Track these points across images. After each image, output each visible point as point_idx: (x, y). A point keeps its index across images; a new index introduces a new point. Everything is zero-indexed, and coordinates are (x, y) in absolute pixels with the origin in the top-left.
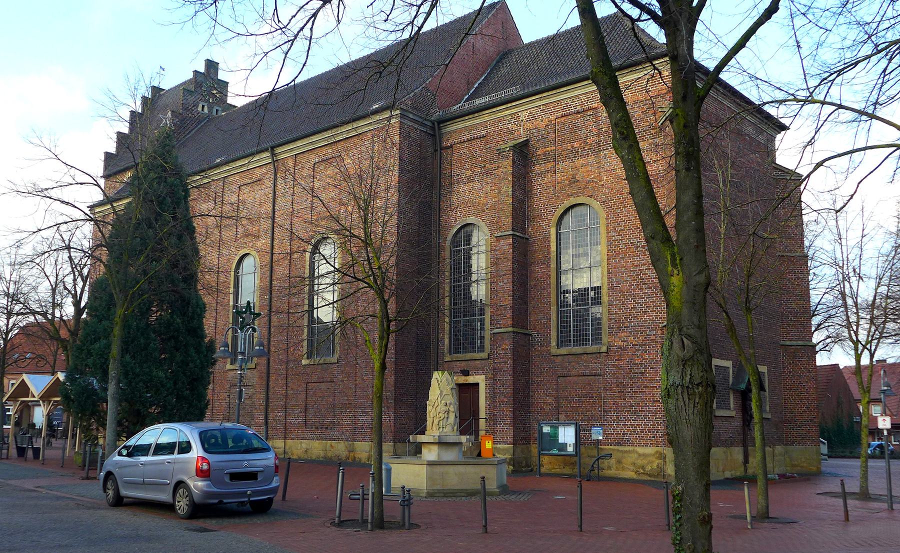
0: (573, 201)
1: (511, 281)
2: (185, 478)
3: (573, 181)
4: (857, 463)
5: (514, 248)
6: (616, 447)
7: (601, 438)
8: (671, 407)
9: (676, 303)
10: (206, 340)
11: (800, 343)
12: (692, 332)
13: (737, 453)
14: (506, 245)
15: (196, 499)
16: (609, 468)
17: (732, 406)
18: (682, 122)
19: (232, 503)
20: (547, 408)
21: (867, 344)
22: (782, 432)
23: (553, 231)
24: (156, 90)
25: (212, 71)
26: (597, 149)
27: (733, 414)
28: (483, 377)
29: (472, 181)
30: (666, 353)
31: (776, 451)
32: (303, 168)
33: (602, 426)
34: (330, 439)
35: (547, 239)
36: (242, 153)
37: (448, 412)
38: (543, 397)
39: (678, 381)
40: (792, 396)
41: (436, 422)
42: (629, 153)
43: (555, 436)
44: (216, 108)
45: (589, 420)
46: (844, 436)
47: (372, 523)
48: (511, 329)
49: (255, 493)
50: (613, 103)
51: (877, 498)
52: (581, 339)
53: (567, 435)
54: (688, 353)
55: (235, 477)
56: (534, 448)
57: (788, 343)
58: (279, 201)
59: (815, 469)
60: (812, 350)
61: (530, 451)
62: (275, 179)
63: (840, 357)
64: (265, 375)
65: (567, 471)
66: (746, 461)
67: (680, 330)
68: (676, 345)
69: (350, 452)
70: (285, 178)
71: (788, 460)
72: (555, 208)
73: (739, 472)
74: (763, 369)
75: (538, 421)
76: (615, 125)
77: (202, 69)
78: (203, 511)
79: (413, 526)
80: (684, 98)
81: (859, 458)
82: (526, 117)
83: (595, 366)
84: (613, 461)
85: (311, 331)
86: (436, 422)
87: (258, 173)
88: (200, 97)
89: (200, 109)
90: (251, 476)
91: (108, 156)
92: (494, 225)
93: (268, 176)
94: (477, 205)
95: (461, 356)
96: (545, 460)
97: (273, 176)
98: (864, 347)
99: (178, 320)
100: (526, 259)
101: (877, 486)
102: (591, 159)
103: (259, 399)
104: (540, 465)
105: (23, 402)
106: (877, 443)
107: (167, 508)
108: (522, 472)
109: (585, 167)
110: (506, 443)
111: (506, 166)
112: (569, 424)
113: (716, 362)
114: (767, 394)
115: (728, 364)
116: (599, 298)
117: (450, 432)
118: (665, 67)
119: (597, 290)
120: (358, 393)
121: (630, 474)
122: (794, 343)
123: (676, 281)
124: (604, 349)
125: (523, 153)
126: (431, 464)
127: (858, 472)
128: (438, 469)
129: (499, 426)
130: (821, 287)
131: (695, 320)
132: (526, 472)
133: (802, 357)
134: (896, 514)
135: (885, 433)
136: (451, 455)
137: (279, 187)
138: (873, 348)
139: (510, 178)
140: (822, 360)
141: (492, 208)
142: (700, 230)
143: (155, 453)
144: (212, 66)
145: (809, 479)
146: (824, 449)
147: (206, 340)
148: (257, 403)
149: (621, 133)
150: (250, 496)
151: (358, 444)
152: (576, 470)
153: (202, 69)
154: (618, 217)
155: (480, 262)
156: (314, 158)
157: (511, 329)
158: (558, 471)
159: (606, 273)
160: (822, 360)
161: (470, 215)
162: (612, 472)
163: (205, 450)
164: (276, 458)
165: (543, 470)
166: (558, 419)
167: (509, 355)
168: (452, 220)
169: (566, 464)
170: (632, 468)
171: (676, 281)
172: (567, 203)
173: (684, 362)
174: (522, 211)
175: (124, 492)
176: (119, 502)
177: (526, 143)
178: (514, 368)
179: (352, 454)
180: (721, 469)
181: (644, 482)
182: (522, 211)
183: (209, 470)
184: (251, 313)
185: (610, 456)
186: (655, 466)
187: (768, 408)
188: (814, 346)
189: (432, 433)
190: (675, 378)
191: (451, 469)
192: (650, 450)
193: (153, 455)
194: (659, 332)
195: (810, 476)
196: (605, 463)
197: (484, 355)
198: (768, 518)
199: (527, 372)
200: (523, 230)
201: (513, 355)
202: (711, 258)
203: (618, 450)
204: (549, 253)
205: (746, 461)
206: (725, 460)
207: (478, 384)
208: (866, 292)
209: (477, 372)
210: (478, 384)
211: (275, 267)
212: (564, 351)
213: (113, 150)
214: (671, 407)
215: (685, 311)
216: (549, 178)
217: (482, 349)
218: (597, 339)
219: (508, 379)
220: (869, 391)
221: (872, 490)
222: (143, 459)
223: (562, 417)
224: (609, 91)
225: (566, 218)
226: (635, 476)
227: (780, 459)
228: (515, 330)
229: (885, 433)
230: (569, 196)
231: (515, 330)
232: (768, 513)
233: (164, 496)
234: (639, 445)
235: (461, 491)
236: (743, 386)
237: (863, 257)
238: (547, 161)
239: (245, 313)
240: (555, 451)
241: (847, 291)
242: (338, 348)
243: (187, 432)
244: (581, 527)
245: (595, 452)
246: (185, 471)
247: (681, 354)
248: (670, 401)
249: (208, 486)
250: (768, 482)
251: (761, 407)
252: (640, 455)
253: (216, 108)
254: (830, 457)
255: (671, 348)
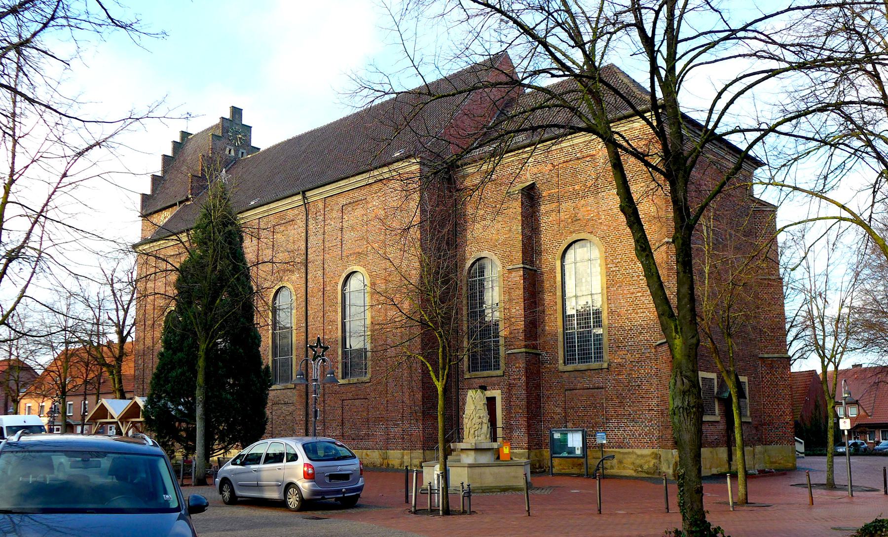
0: (575, 237)
1: (522, 307)
2: (295, 480)
3: (575, 220)
4: (824, 460)
5: (524, 279)
6: (618, 450)
7: (605, 442)
8: (676, 421)
9: (678, 356)
10: (263, 367)
11: (776, 355)
12: (688, 374)
13: (722, 452)
14: (517, 277)
15: (305, 495)
16: (612, 468)
17: (717, 412)
18: (681, 242)
19: (333, 498)
20: (557, 417)
21: (832, 357)
22: (758, 434)
23: (558, 263)
24: (185, 135)
25: (237, 116)
26: (596, 190)
27: (718, 419)
28: (499, 391)
29: (485, 219)
30: (672, 387)
31: (756, 450)
32: (332, 210)
33: (605, 431)
34: (365, 449)
35: (553, 270)
36: (274, 197)
37: (482, 423)
38: (553, 408)
39: (680, 405)
40: (770, 402)
41: (472, 432)
42: (646, 260)
43: (565, 441)
44: (241, 150)
45: (593, 427)
46: (816, 435)
47: (443, 510)
48: (523, 350)
49: (348, 491)
50: (635, 226)
51: (843, 488)
52: (585, 357)
53: (575, 440)
54: (686, 388)
55: (333, 477)
56: (546, 453)
57: (766, 356)
58: (310, 239)
59: (791, 465)
60: (788, 361)
61: (542, 455)
62: (307, 220)
63: (812, 363)
64: (304, 394)
65: (575, 471)
66: (730, 458)
67: (681, 373)
68: (679, 383)
69: (383, 459)
70: (315, 219)
71: (767, 458)
72: (560, 244)
73: (723, 470)
74: (743, 379)
75: (549, 429)
76: (637, 241)
77: (228, 115)
78: (307, 505)
79: (472, 513)
80: (681, 227)
81: (826, 455)
82: (531, 165)
83: (598, 380)
84: (615, 461)
85: (345, 353)
86: (472, 432)
87: (291, 214)
88: (227, 141)
89: (227, 152)
90: (345, 477)
91: (145, 197)
92: (506, 258)
93: (300, 217)
94: (491, 240)
95: (479, 374)
96: (556, 462)
97: (304, 217)
98: (830, 360)
99: (241, 350)
100: (534, 286)
101: (841, 478)
102: (591, 200)
103: (300, 415)
104: (552, 467)
105: (132, 422)
106: (853, 441)
107: (281, 504)
108: (537, 473)
109: (587, 207)
110: (522, 448)
111: (515, 207)
112: (577, 431)
113: (702, 374)
114: (748, 401)
115: (713, 376)
116: (600, 321)
117: (484, 440)
118: (635, 33)
119: (597, 313)
120: (390, 408)
121: (630, 472)
122: (770, 355)
123: (678, 342)
124: (605, 365)
125: (531, 195)
126: (471, 466)
127: (825, 467)
128: (477, 470)
129: (515, 434)
130: (793, 306)
131: (690, 366)
132: (540, 472)
133: (779, 368)
134: (854, 499)
135: (846, 433)
136: (485, 458)
137: (310, 227)
138: (837, 361)
139: (520, 218)
140: (795, 368)
141: (504, 244)
142: (693, 310)
143: (266, 462)
144: (237, 112)
145: (785, 474)
146: (800, 448)
147: (263, 367)
148: (298, 418)
149: (641, 247)
150: (344, 493)
151: (390, 452)
152: (584, 470)
153: (228, 115)
154: (615, 251)
155: (493, 295)
156: (342, 201)
157: (523, 350)
158: (567, 471)
159: (605, 300)
160: (795, 368)
161: (482, 250)
162: (615, 471)
163: (310, 459)
164: (361, 463)
165: (554, 470)
166: (566, 426)
167: (523, 372)
168: (467, 254)
169: (574, 465)
170: (632, 467)
171: (678, 342)
172: (570, 239)
173: (684, 393)
174: (531, 248)
175: (239, 493)
176: (234, 501)
177: (532, 187)
178: (527, 383)
179: (386, 461)
180: (708, 466)
181: (642, 479)
182: (531, 248)
183: (313, 474)
184: (321, 347)
185: (613, 457)
186: (651, 465)
187: (748, 414)
188: (789, 358)
189: (469, 441)
190: (678, 403)
191: (487, 470)
192: (647, 451)
193: (265, 463)
194: (653, 350)
195: (784, 472)
196: (608, 464)
197: (499, 373)
198: (747, 503)
199: (538, 386)
200: (532, 263)
201: (526, 372)
202: (698, 290)
203: (619, 452)
204: (555, 283)
205: (730, 458)
206: (713, 458)
207: (494, 398)
208: (832, 312)
209: (494, 386)
210: (494, 398)
211: (309, 298)
212: (570, 367)
213: (148, 192)
214: (676, 421)
215: (684, 361)
216: (553, 217)
217: (497, 367)
218: (599, 357)
219: (521, 392)
220: (834, 398)
221: (837, 482)
222: (253, 467)
223: (570, 425)
224: (632, 219)
225: (568, 251)
226: (634, 474)
227: (760, 456)
228: (527, 350)
229: (846, 433)
230: (571, 232)
231: (527, 350)
232: (747, 499)
233: (275, 495)
234: (638, 447)
235: (495, 487)
236: (726, 395)
237: (829, 284)
238: (551, 201)
239: (316, 347)
240: (565, 454)
241: (815, 313)
242: (369, 370)
243: (295, 445)
244: (600, 510)
245: (599, 454)
246: (295, 476)
247: (682, 388)
248: (675, 417)
249: (313, 486)
250: (748, 476)
251: (740, 415)
252: (638, 456)
253: (241, 150)
254: (806, 455)
255: (675, 384)
